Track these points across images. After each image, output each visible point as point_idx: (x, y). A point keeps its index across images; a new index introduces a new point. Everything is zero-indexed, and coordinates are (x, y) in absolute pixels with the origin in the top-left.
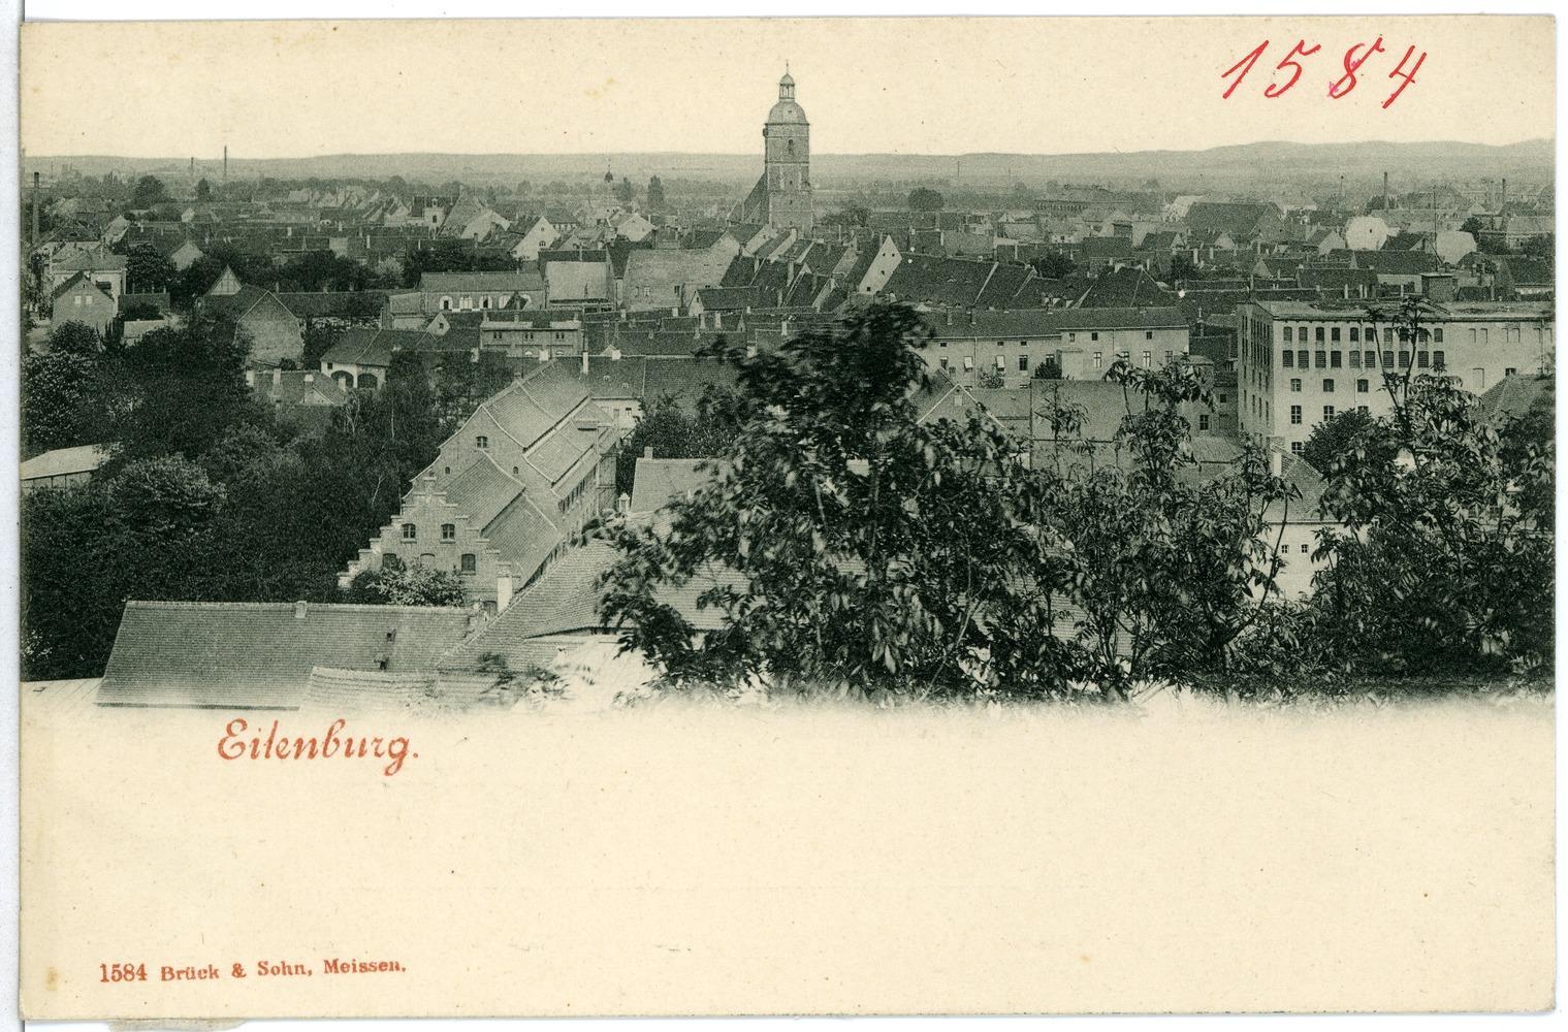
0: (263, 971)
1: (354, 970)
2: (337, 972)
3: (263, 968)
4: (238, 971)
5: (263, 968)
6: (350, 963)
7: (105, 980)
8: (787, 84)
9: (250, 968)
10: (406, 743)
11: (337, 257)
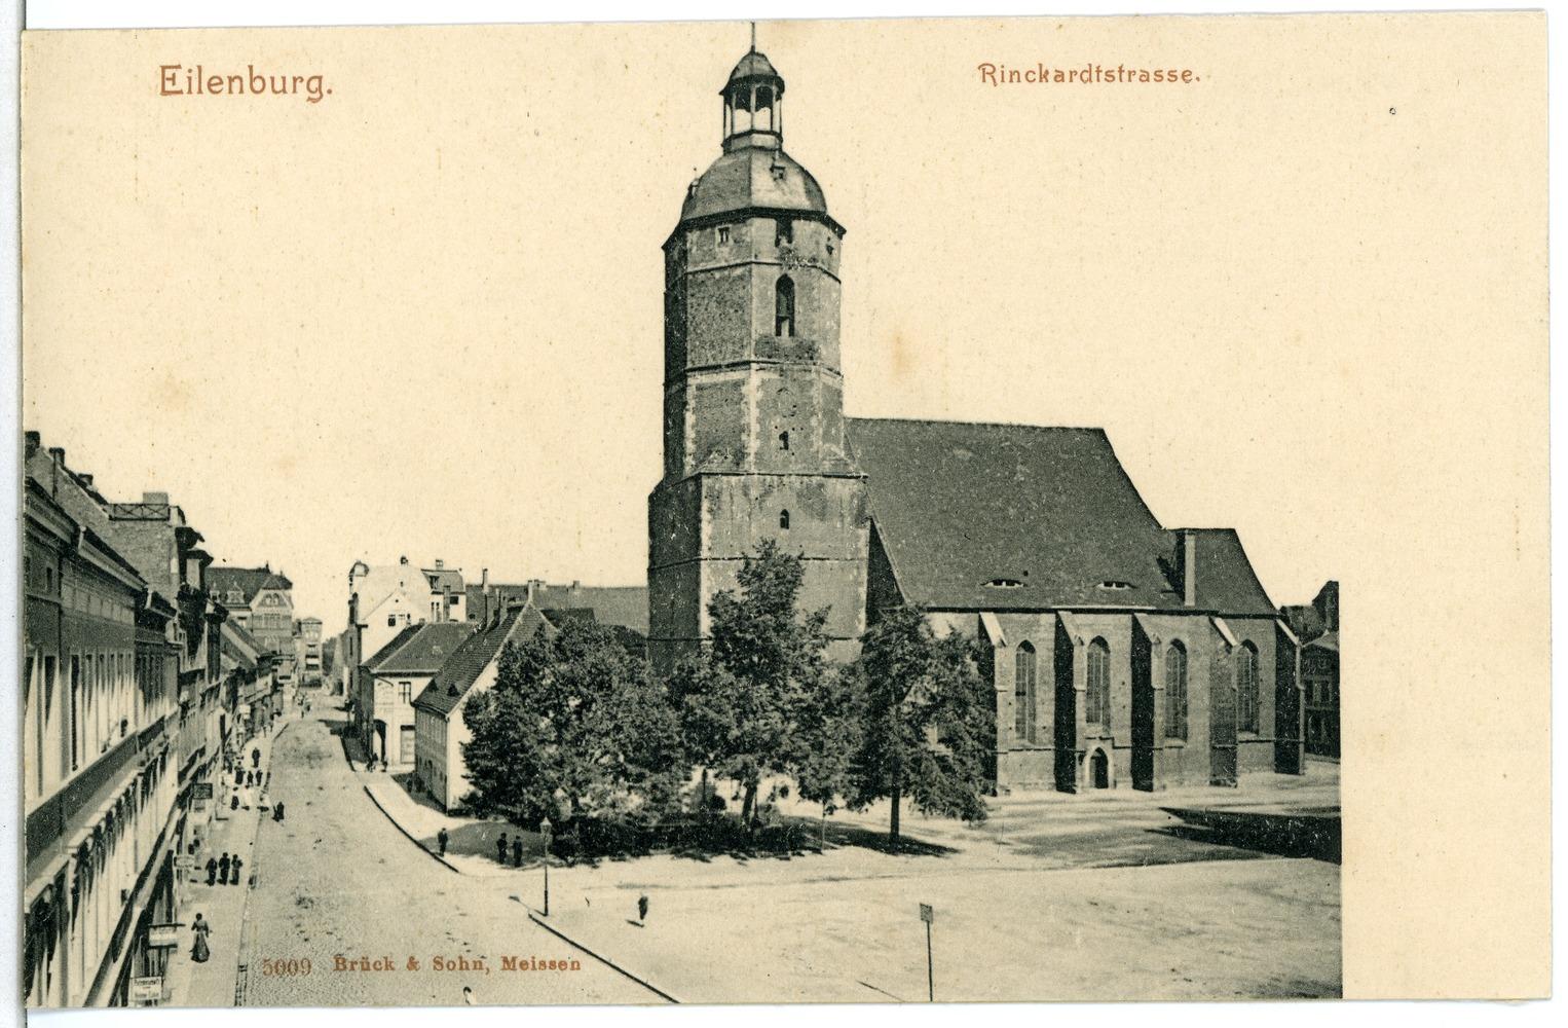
0: (438, 967)
1: (534, 968)
2: (514, 969)
3: (438, 962)
4: (412, 964)
5: (438, 962)
7: (337, 969)
8: (829, 608)
9: (425, 961)
10: (320, 78)
11: (688, 234)
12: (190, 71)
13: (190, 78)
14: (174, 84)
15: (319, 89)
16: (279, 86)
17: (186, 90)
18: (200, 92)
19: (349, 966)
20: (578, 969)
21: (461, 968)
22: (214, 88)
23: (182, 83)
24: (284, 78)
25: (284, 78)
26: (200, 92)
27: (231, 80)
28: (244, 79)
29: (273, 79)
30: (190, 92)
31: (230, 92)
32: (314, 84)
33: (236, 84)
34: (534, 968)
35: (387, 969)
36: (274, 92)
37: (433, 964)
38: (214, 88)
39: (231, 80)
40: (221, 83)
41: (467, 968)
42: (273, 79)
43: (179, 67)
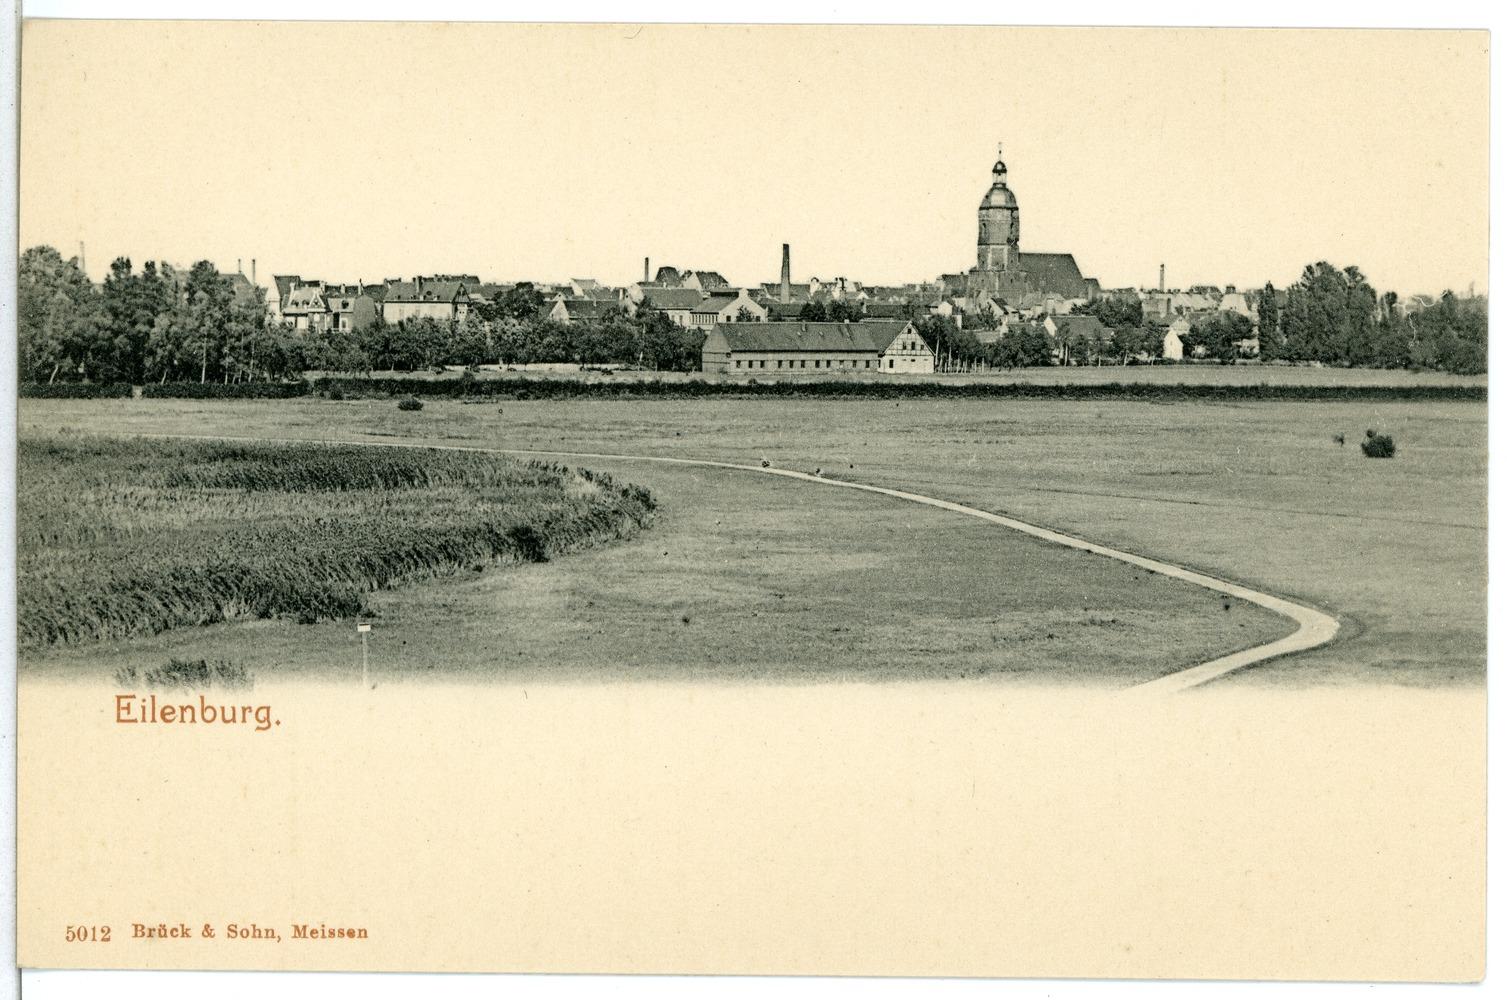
0: (233, 934)
3: (232, 930)
4: (208, 931)
5: (232, 930)
6: (319, 929)
7: (136, 935)
9: (220, 930)
12: (144, 701)
13: (144, 708)
14: (129, 713)
15: (267, 718)
16: (229, 716)
17: (140, 719)
18: (154, 720)
19: (147, 933)
20: (366, 936)
21: (254, 936)
22: (167, 717)
23: (136, 713)
24: (234, 709)
25: (234, 709)
26: (154, 720)
27: (183, 709)
28: (196, 709)
29: (223, 709)
30: (144, 720)
31: (182, 721)
32: (263, 714)
34: (323, 937)
35: (183, 936)
36: (225, 721)
37: (227, 931)
38: (167, 717)
39: (183, 709)
40: (174, 712)
41: (260, 936)
42: (223, 709)
43: (134, 697)
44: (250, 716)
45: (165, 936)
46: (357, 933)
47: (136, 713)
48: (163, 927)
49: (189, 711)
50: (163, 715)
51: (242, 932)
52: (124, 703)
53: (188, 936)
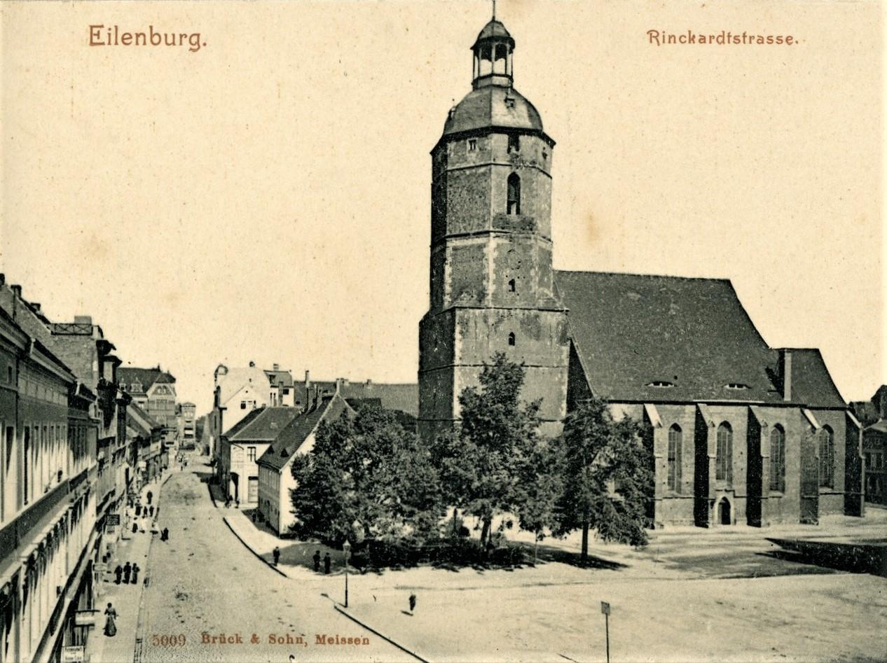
4: (255, 639)
6: (335, 638)
7: (204, 642)
13: (109, 34)
14: (98, 38)
15: (198, 43)
16: (170, 40)
17: (107, 42)
18: (116, 43)
20: (368, 643)
21: (288, 642)
22: (126, 41)
23: (104, 38)
24: (174, 35)
25: (174, 35)
26: (116, 43)
27: (138, 35)
29: (166, 35)
30: (109, 43)
31: (137, 44)
32: (194, 39)
33: (141, 38)
34: (338, 643)
38: (126, 41)
39: (138, 35)
40: (131, 37)
41: (292, 643)
42: (166, 35)
44: (186, 41)
45: (224, 642)
46: (362, 641)
47: (104, 38)
48: (223, 635)
49: (142, 37)
50: (123, 39)
51: (279, 641)
52: (95, 31)
53: (241, 642)
